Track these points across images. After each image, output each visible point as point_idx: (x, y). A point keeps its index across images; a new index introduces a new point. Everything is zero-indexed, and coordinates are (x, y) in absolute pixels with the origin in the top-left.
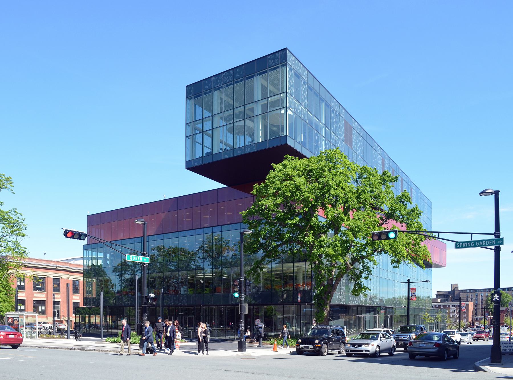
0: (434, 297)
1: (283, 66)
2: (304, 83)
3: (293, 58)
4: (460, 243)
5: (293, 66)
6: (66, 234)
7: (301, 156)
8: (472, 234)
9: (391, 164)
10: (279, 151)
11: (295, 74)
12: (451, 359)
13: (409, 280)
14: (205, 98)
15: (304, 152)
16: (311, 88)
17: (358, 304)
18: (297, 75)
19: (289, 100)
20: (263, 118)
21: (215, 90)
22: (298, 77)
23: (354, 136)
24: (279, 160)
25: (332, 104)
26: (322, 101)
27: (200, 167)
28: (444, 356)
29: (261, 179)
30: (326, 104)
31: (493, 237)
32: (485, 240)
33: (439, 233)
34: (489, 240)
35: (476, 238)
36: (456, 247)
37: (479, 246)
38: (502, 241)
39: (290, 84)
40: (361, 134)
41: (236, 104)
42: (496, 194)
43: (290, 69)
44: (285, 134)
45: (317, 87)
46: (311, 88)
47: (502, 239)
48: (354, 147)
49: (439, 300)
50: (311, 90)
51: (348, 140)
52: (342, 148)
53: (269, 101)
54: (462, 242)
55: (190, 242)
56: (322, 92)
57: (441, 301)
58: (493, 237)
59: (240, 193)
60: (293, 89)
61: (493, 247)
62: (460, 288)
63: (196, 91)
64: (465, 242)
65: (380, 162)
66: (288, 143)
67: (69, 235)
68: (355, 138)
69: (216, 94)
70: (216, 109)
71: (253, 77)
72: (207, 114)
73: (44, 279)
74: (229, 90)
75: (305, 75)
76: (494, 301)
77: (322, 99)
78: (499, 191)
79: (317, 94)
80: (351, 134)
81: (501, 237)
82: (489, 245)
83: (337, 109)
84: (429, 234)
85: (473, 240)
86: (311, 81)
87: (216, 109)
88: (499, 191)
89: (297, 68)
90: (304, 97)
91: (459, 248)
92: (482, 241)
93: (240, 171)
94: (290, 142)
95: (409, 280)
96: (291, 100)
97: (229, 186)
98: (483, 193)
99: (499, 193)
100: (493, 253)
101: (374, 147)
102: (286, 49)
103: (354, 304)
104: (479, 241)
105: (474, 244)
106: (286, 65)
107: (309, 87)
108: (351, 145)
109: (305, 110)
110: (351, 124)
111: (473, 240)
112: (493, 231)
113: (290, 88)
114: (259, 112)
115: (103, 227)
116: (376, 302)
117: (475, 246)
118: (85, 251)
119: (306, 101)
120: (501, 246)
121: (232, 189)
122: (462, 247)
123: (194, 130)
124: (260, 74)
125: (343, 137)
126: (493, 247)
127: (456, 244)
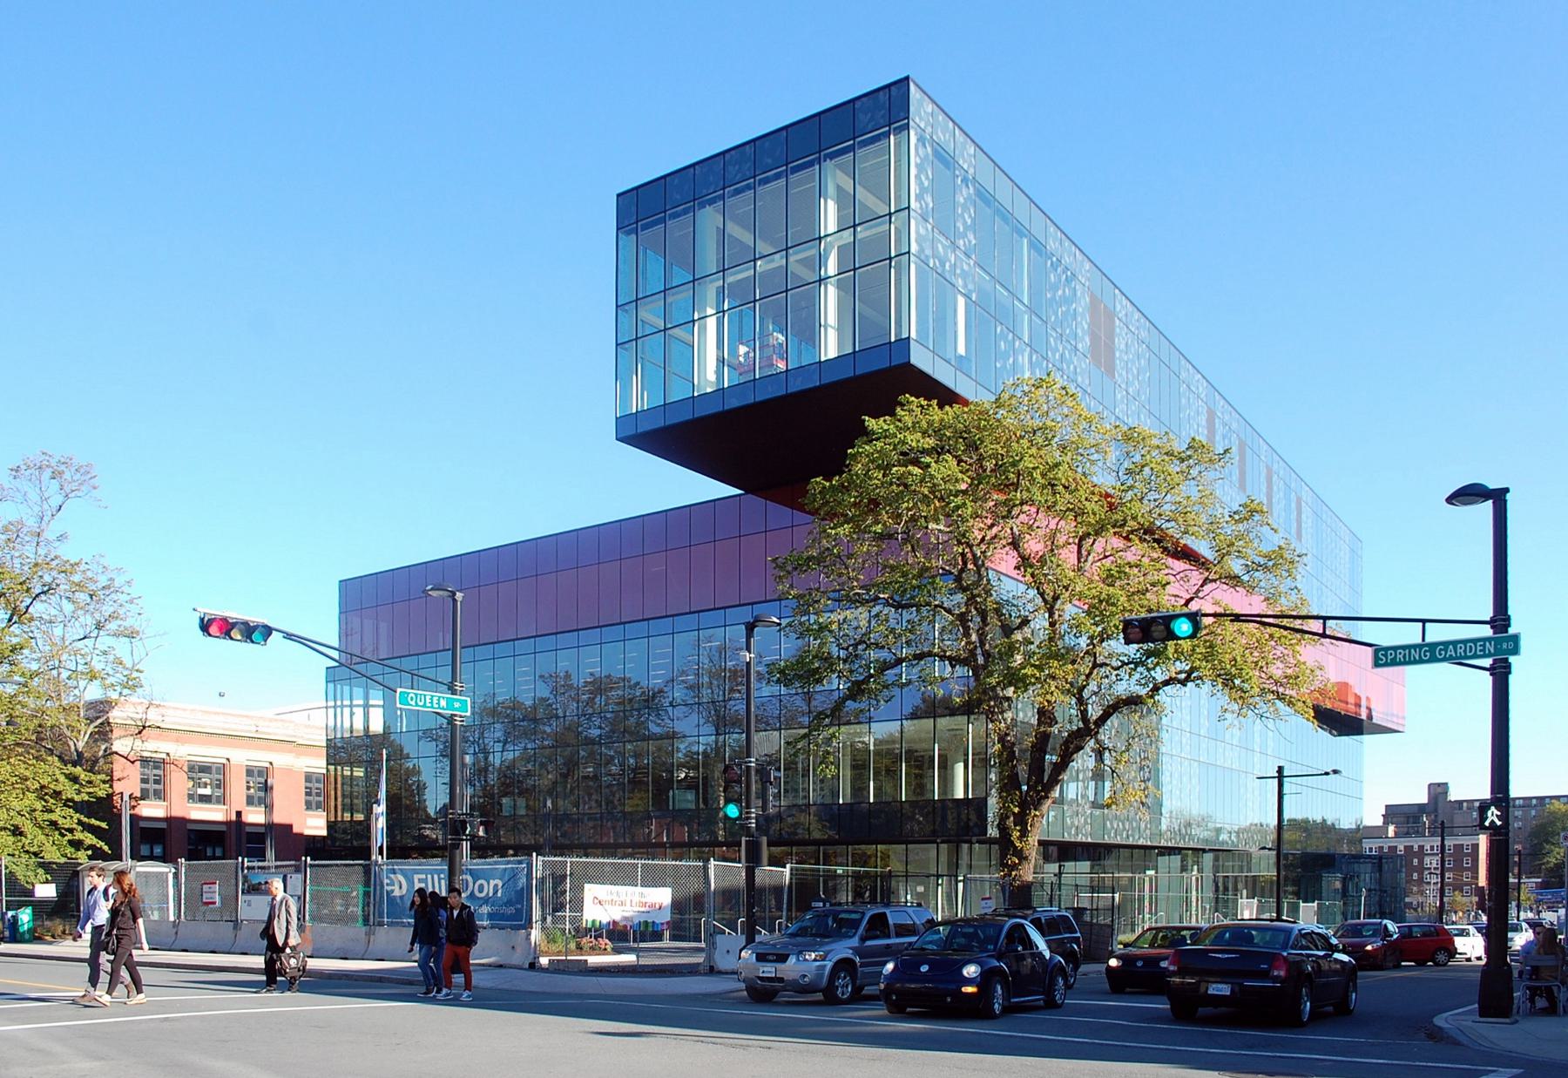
0: (1379, 822)
1: (899, 130)
2: (965, 180)
3: (930, 108)
4: (1387, 649)
5: (929, 130)
6: (205, 627)
7: (947, 397)
8: (1424, 621)
9: (1234, 426)
10: (888, 379)
11: (936, 153)
12: (1327, 1015)
13: (1280, 769)
14: (677, 228)
15: (962, 387)
16: (984, 197)
17: (1131, 842)
18: (943, 158)
19: (917, 232)
20: (849, 290)
21: (702, 206)
22: (946, 164)
23: (1120, 343)
24: (887, 408)
25: (1052, 245)
26: (1021, 235)
27: (679, 436)
28: (1300, 1012)
29: (835, 464)
30: (1031, 245)
31: (1487, 631)
32: (1465, 642)
33: (1325, 619)
34: (1475, 641)
35: (1436, 634)
36: (1377, 664)
37: (1444, 660)
38: (1514, 645)
39: (920, 184)
40: (1144, 334)
41: (763, 248)
42: (1498, 497)
43: (921, 140)
44: (905, 336)
45: (1004, 193)
46: (984, 197)
47: (1515, 638)
48: (1120, 373)
49: (1391, 830)
50: (987, 203)
51: (1103, 354)
52: (1080, 370)
53: (859, 236)
54: (1395, 648)
55: (646, 659)
56: (1022, 210)
57: (1397, 835)
58: (1487, 631)
59: (780, 513)
60: (929, 199)
61: (1487, 662)
62: (1454, 795)
63: (649, 209)
64: (1403, 647)
65: (1203, 419)
66: (913, 361)
67: (214, 629)
68: (1123, 347)
69: (709, 218)
70: (709, 259)
71: (811, 164)
72: (680, 276)
73: (223, 769)
74: (741, 204)
75: (967, 156)
76: (1486, 828)
77: (1019, 230)
78: (1507, 490)
79: (1005, 215)
80: (1111, 336)
81: (1511, 631)
82: (1475, 656)
83: (1067, 260)
84: (1297, 624)
85: (1428, 640)
86: (987, 176)
87: (709, 259)
88: (1507, 490)
89: (940, 136)
90: (965, 222)
91: (1386, 665)
92: (1454, 643)
93: (786, 444)
94: (920, 359)
95: (1280, 769)
96: (922, 231)
97: (747, 492)
98: (1467, 495)
99: (1508, 496)
100: (1486, 680)
101: (1183, 375)
102: (907, 78)
103: (1119, 841)
104: (1446, 644)
105: (1429, 653)
106: (907, 127)
107: (978, 193)
108: (1110, 370)
109: (967, 265)
110: (1110, 306)
111: (1428, 640)
112: (1488, 614)
113: (919, 198)
114: (832, 267)
115: (395, 618)
116: (1199, 836)
117: (1433, 659)
118: (331, 686)
119: (971, 237)
120: (1512, 659)
121: (756, 501)
122: (1394, 663)
123: (644, 325)
124: (832, 156)
125: (1084, 344)
126: (1487, 662)
127: (1376, 653)
